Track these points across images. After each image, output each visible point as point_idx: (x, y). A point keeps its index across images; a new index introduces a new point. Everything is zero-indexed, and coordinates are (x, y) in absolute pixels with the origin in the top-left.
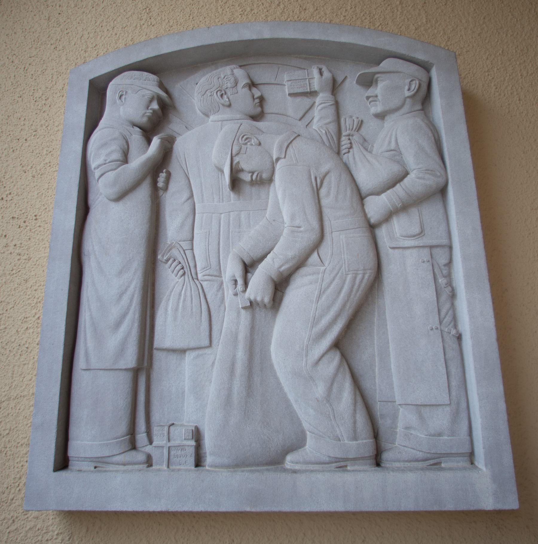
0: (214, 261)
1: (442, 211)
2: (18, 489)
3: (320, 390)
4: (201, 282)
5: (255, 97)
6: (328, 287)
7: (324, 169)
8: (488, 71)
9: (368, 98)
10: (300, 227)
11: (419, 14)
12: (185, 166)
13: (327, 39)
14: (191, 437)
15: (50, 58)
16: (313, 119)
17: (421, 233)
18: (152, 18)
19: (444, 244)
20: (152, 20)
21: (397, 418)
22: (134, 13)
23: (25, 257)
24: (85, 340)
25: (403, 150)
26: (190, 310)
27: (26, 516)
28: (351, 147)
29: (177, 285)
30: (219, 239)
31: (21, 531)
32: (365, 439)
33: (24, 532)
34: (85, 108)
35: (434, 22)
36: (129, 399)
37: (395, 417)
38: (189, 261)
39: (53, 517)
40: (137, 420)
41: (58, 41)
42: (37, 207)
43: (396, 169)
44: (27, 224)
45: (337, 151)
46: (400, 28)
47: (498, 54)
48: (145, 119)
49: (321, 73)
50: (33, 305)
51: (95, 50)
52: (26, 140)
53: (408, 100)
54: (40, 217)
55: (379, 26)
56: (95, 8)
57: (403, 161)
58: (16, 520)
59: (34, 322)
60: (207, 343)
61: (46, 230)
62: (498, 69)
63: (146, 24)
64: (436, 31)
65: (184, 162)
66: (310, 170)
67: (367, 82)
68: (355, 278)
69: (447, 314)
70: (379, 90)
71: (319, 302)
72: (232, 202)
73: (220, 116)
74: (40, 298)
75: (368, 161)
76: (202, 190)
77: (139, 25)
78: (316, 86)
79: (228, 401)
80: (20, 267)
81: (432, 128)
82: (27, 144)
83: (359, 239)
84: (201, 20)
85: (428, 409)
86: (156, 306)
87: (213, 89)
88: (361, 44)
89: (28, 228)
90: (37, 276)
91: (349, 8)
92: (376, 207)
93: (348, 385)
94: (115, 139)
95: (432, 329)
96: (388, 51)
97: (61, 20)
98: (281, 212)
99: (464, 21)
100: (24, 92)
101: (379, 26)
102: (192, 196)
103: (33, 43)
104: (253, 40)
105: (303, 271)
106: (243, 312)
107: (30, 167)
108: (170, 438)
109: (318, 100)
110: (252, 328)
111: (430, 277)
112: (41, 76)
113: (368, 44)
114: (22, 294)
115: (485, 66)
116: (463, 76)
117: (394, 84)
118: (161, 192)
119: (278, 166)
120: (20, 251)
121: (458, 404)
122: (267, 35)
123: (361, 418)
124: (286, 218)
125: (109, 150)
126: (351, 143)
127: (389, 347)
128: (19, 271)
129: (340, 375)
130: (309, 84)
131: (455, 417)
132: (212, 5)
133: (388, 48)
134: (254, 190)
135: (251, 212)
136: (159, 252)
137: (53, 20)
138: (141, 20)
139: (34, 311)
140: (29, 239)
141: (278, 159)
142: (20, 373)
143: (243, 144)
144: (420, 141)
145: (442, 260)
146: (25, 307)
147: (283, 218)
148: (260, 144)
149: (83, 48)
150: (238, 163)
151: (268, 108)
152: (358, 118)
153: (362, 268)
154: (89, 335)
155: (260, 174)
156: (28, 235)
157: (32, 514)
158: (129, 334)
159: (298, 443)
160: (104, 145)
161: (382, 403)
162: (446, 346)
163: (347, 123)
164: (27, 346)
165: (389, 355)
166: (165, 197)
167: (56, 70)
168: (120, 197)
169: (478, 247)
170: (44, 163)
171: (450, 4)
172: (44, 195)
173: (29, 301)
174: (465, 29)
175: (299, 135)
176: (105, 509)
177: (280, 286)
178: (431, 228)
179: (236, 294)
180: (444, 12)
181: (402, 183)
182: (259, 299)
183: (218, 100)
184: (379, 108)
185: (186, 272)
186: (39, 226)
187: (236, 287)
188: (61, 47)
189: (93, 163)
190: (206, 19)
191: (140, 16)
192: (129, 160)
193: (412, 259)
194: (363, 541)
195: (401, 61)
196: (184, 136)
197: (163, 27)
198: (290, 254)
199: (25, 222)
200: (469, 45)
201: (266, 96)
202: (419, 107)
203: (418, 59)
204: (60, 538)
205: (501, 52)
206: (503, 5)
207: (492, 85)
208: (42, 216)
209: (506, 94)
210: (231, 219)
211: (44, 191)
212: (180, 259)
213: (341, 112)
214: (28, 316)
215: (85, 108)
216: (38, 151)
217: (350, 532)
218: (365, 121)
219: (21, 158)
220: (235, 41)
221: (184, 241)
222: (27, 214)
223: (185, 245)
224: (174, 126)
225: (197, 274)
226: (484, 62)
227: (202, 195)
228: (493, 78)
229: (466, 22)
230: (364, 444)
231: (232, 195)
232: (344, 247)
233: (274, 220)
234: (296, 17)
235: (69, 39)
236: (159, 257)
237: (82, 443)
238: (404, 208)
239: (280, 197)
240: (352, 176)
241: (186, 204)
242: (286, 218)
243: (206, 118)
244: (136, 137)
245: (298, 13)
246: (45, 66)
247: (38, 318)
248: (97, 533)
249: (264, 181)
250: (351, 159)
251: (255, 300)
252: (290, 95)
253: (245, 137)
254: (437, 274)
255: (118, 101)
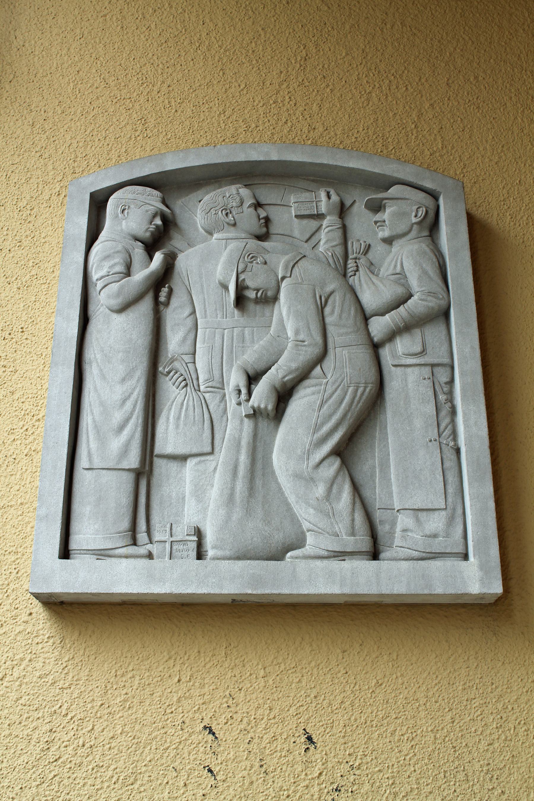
0: (217, 373)
1: (444, 332)
2: (6, 595)
3: (320, 490)
4: (204, 394)
5: (261, 217)
6: (331, 397)
7: (329, 288)
8: (503, 200)
9: (376, 222)
10: (304, 341)
11: (435, 139)
12: (187, 282)
13: (335, 164)
14: (193, 533)
15: (35, 167)
16: (320, 241)
17: (423, 352)
18: (148, 129)
19: (445, 362)
20: (148, 132)
21: (396, 524)
22: (128, 124)
23: (11, 369)
24: (88, 441)
25: (408, 274)
26: (192, 418)
27: (15, 621)
28: (357, 270)
29: (179, 396)
30: (223, 353)
31: (10, 635)
32: (363, 536)
33: (13, 636)
34: (86, 220)
35: (450, 148)
36: (132, 498)
37: (394, 524)
38: (191, 374)
39: (44, 621)
40: (138, 520)
41: (43, 149)
42: (23, 319)
43: (400, 291)
44: (12, 336)
45: (343, 274)
46: (415, 152)
47: (515, 183)
48: (148, 234)
49: (329, 197)
50: (20, 417)
51: (86, 160)
52: (10, 251)
53: (415, 226)
54: (27, 330)
55: (392, 150)
56: (84, 116)
57: (409, 285)
58: (5, 624)
59: (22, 433)
60: (208, 449)
61: (33, 343)
62: (514, 199)
63: (141, 136)
64: (452, 157)
65: (186, 278)
66: (315, 288)
67: (376, 207)
68: (356, 391)
69: (446, 428)
70: (386, 215)
71: (321, 411)
72: (236, 318)
73: (224, 234)
74: (28, 411)
75: (374, 283)
76: (205, 306)
77: (133, 136)
78: (323, 209)
79: (230, 499)
80: (6, 379)
81: (437, 254)
82: (11, 255)
83: (363, 355)
84: (202, 134)
85: (425, 513)
86: (156, 416)
87: (218, 208)
88: (370, 170)
89: (14, 340)
90: (24, 388)
91: (362, 129)
92: (378, 326)
93: (347, 488)
94: (118, 252)
95: (431, 441)
96: (396, 178)
97: (46, 126)
98: (285, 329)
99: (481, 149)
100: (6, 200)
101: (392, 150)
102: (194, 312)
103: (15, 149)
104: (260, 161)
105: (307, 382)
106: (246, 420)
107: (14, 278)
108: (173, 533)
109: (325, 223)
110: (255, 436)
111: (431, 393)
112: (25, 185)
113: (377, 170)
114: (8, 405)
115: (501, 195)
116: (478, 204)
117: (402, 210)
118: (162, 307)
119: (284, 285)
120: (5, 363)
121: (454, 509)
122: (274, 157)
123: (359, 517)
124: (290, 333)
125: (112, 262)
126: (357, 266)
127: (389, 459)
128: (5, 383)
129: (340, 478)
130: (317, 206)
131: (451, 520)
132: (213, 119)
133: (395, 175)
134: (258, 307)
135: (255, 329)
136: (160, 364)
137: (38, 126)
138: (136, 131)
139: (21, 423)
140: (16, 351)
141: (283, 278)
142: (6, 484)
143: (249, 262)
144: (424, 265)
145: (443, 376)
146: (12, 419)
147: (287, 334)
148: (266, 263)
149: (72, 158)
150: (244, 280)
151: (274, 229)
152: (365, 242)
153: (364, 381)
154: (91, 437)
155: (265, 291)
156: (14, 347)
157: (21, 619)
158: (132, 436)
159: (299, 543)
160: (107, 257)
161: (382, 510)
162: (444, 457)
163: (354, 247)
164: (14, 457)
165: (390, 467)
166: (166, 312)
167: (42, 180)
168: (123, 309)
169: (476, 365)
170: (31, 274)
171: (468, 131)
172: (30, 308)
173: (16, 413)
174: (483, 156)
175: (305, 256)
176: (111, 592)
177: (283, 396)
178: (433, 348)
179: (239, 404)
180: (461, 138)
181: (405, 305)
182: (262, 406)
183: (223, 218)
184: (385, 233)
185: (189, 383)
186: (26, 339)
187: (239, 397)
188: (47, 155)
189: (95, 275)
190: (207, 134)
191: (135, 127)
192: (132, 274)
193: (413, 375)
194: (361, 645)
195: (409, 188)
196: (186, 253)
197: (160, 140)
198: (294, 365)
199: (10, 334)
200: (485, 174)
201: (271, 217)
202: (426, 233)
203: (425, 187)
204: (50, 643)
205: (518, 181)
206: (522, 134)
207: (508, 214)
208: (29, 329)
209: (522, 225)
210: (235, 334)
211: (30, 304)
212: (183, 372)
213: (348, 235)
214: (15, 428)
215: (87, 220)
216: (23, 262)
217: (348, 637)
218: (372, 245)
219: (4, 269)
220: (242, 161)
221: (186, 354)
222: (11, 326)
223: (187, 358)
224: (176, 242)
225: (199, 386)
226: (500, 191)
227: (206, 311)
228: (509, 208)
229: (484, 150)
230: (363, 542)
231: (236, 312)
232: (346, 364)
233: (278, 336)
234: (305, 136)
235: (56, 147)
236: (160, 369)
237: (84, 536)
238: (406, 328)
239: (284, 313)
240: (357, 297)
241: (188, 319)
242: (290, 333)
243: (209, 236)
244: (139, 251)
245: (306, 132)
246: (29, 174)
247: (27, 430)
248: (90, 636)
249: (269, 299)
250: (357, 282)
251: (259, 407)
252: (296, 216)
253: (251, 256)
254: (438, 390)
255: (120, 215)
